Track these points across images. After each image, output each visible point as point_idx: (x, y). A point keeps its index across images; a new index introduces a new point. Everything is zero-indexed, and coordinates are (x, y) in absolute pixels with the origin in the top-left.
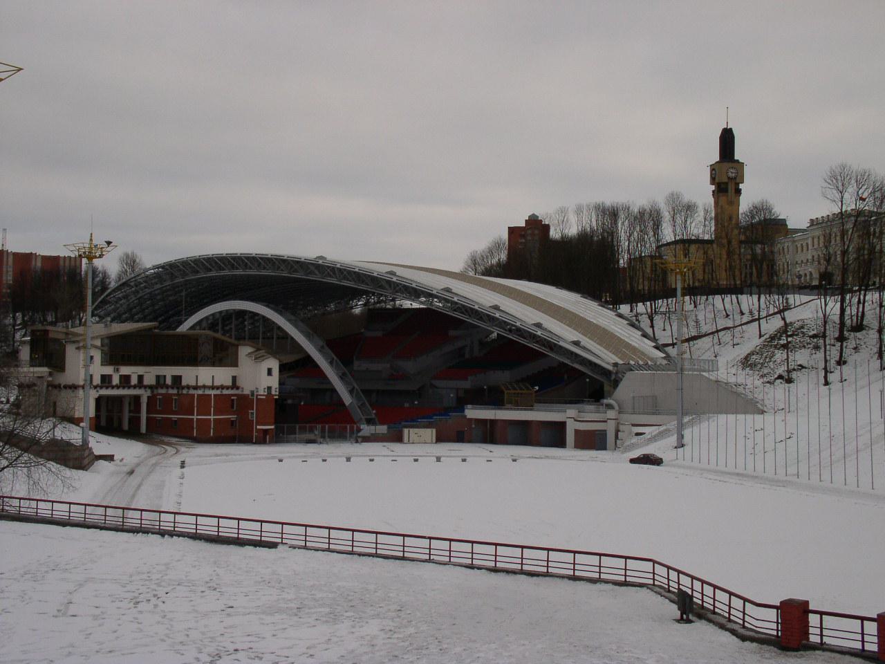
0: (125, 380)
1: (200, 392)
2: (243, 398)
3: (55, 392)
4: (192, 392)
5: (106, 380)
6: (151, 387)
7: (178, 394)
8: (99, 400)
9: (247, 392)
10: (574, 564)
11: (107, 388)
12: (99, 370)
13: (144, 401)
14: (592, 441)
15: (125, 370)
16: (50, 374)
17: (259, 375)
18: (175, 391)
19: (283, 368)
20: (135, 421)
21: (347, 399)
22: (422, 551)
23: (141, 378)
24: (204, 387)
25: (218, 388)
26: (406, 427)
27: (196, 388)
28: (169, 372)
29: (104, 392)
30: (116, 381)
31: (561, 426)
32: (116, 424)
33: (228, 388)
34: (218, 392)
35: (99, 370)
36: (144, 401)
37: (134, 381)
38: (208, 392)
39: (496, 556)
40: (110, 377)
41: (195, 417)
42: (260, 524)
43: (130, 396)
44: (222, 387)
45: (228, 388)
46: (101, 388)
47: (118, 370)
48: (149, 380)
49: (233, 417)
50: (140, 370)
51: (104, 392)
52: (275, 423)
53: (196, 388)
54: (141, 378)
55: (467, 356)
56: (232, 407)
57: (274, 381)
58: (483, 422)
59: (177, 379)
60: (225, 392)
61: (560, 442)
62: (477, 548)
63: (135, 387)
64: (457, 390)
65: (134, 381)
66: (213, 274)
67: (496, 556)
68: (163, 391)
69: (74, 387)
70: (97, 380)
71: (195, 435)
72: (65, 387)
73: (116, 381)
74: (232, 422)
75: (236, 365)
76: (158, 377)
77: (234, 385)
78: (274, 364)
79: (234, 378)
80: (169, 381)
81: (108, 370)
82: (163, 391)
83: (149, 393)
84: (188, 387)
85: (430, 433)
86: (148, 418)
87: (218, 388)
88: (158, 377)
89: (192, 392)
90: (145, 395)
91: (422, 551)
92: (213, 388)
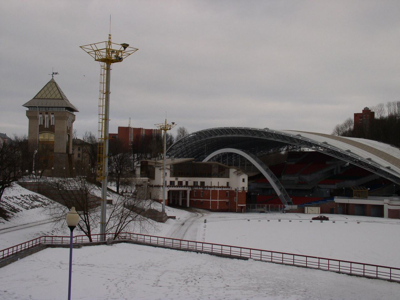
1: (213, 189)
3: (151, 188)
4: (209, 189)
5: (172, 183)
6: (191, 187)
7: (203, 190)
9: (233, 189)
11: (173, 187)
12: (169, 179)
13: (188, 193)
15: (180, 179)
16: (149, 181)
17: (239, 182)
18: (202, 189)
20: (184, 202)
21: (279, 193)
23: (187, 182)
24: (215, 187)
25: (220, 187)
26: (306, 206)
27: (211, 187)
28: (199, 180)
30: (176, 184)
31: (382, 207)
32: (176, 203)
33: (225, 187)
34: (221, 189)
35: (169, 179)
36: (188, 193)
37: (184, 184)
38: (216, 189)
40: (174, 182)
41: (211, 200)
43: (182, 190)
44: (222, 187)
45: (225, 187)
46: (170, 187)
47: (177, 179)
48: (191, 183)
49: (227, 200)
50: (187, 179)
52: (246, 203)
53: (211, 187)
54: (187, 182)
55: (335, 173)
57: (245, 185)
59: (203, 183)
60: (224, 189)
63: (184, 186)
64: (330, 189)
65: (184, 184)
66: (218, 136)
69: (159, 186)
70: (168, 184)
73: (176, 184)
76: (194, 182)
77: (228, 186)
79: (228, 183)
80: (199, 184)
81: (173, 179)
83: (190, 189)
84: (207, 187)
87: (220, 187)
88: (194, 182)
89: (209, 189)
90: (189, 190)
92: (218, 187)
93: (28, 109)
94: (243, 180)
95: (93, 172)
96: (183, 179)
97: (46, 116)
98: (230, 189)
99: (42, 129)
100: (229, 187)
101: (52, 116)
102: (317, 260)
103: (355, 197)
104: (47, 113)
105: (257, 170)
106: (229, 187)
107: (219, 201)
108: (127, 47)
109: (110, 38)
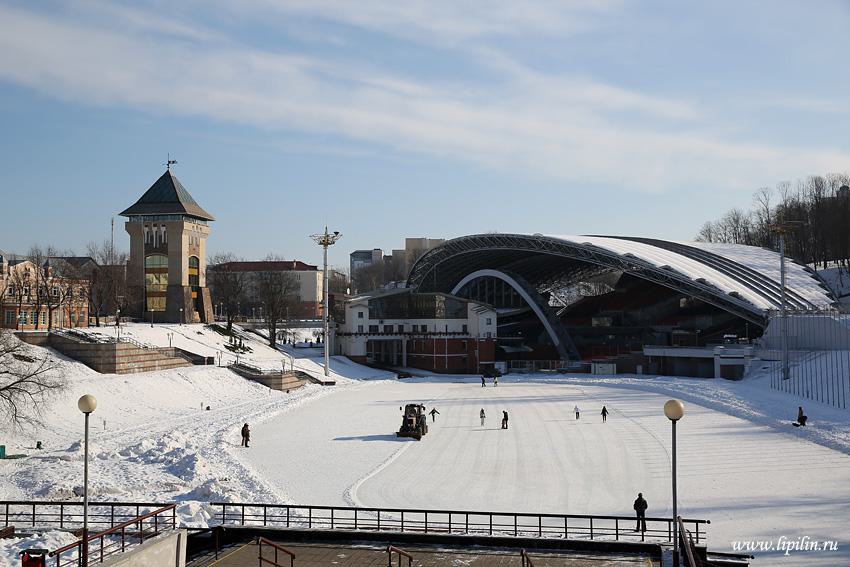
0: (389, 330)
1: (437, 337)
2: (472, 341)
4: (432, 337)
5: (373, 330)
6: (409, 334)
8: (369, 344)
10: (332, 518)
11: (374, 334)
12: (367, 322)
14: (733, 373)
15: (388, 322)
17: (482, 323)
18: (422, 337)
19: (500, 320)
20: (400, 358)
21: (556, 341)
22: (349, 521)
23: (401, 327)
24: (440, 333)
25: (450, 334)
27: (434, 334)
29: (372, 337)
33: (459, 334)
34: (451, 337)
35: (367, 322)
36: (405, 344)
37: (396, 329)
39: (540, 527)
40: (377, 326)
42: (5, 506)
44: (454, 333)
45: (459, 334)
47: (382, 322)
48: (408, 328)
50: (400, 322)
51: (372, 337)
53: (434, 334)
54: (401, 327)
56: (464, 347)
57: (493, 329)
58: (656, 358)
59: (424, 328)
60: (457, 337)
61: (710, 375)
62: (597, 523)
63: (396, 334)
65: (396, 329)
66: (479, 249)
67: (516, 526)
68: (416, 337)
69: (350, 334)
70: (366, 329)
71: (531, 350)
72: (346, 334)
74: (464, 359)
75: (467, 318)
76: (414, 326)
78: (493, 317)
79: (465, 327)
80: (420, 329)
81: (375, 322)
82: (416, 337)
83: (408, 338)
84: (430, 333)
85: (612, 367)
86: (408, 356)
87: (450, 334)
90: (405, 339)
91: (349, 521)
92: (446, 334)
93: (127, 219)
94: (361, 315)
95: (726, 336)
96: (395, 323)
97: (155, 229)
98: (468, 337)
99: (150, 250)
100: (468, 334)
101: (163, 229)
102: (398, 516)
103: (676, 346)
104: (155, 226)
105: (526, 304)
106: (468, 334)
107: (444, 353)
108: (778, 251)
109: (346, 334)
